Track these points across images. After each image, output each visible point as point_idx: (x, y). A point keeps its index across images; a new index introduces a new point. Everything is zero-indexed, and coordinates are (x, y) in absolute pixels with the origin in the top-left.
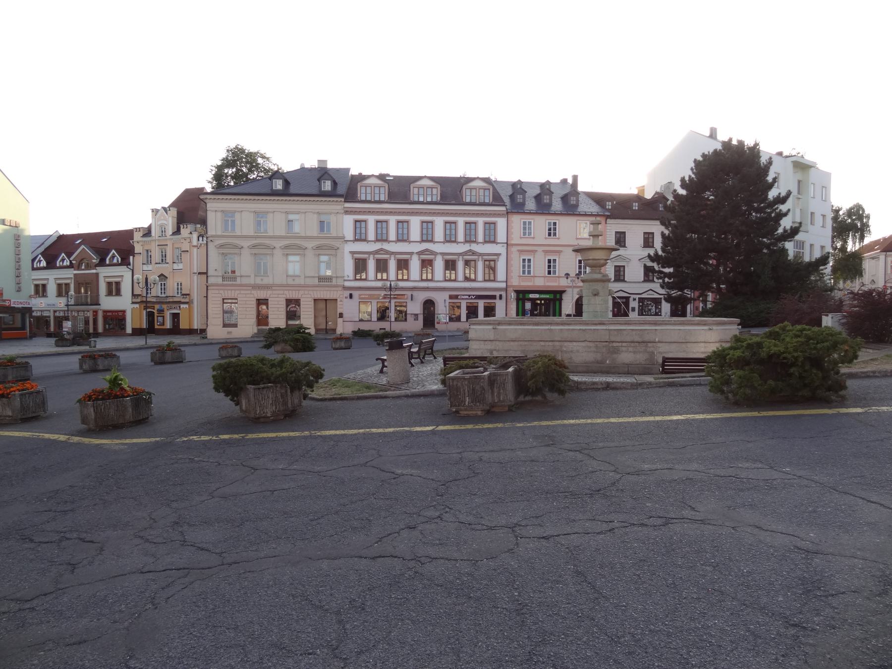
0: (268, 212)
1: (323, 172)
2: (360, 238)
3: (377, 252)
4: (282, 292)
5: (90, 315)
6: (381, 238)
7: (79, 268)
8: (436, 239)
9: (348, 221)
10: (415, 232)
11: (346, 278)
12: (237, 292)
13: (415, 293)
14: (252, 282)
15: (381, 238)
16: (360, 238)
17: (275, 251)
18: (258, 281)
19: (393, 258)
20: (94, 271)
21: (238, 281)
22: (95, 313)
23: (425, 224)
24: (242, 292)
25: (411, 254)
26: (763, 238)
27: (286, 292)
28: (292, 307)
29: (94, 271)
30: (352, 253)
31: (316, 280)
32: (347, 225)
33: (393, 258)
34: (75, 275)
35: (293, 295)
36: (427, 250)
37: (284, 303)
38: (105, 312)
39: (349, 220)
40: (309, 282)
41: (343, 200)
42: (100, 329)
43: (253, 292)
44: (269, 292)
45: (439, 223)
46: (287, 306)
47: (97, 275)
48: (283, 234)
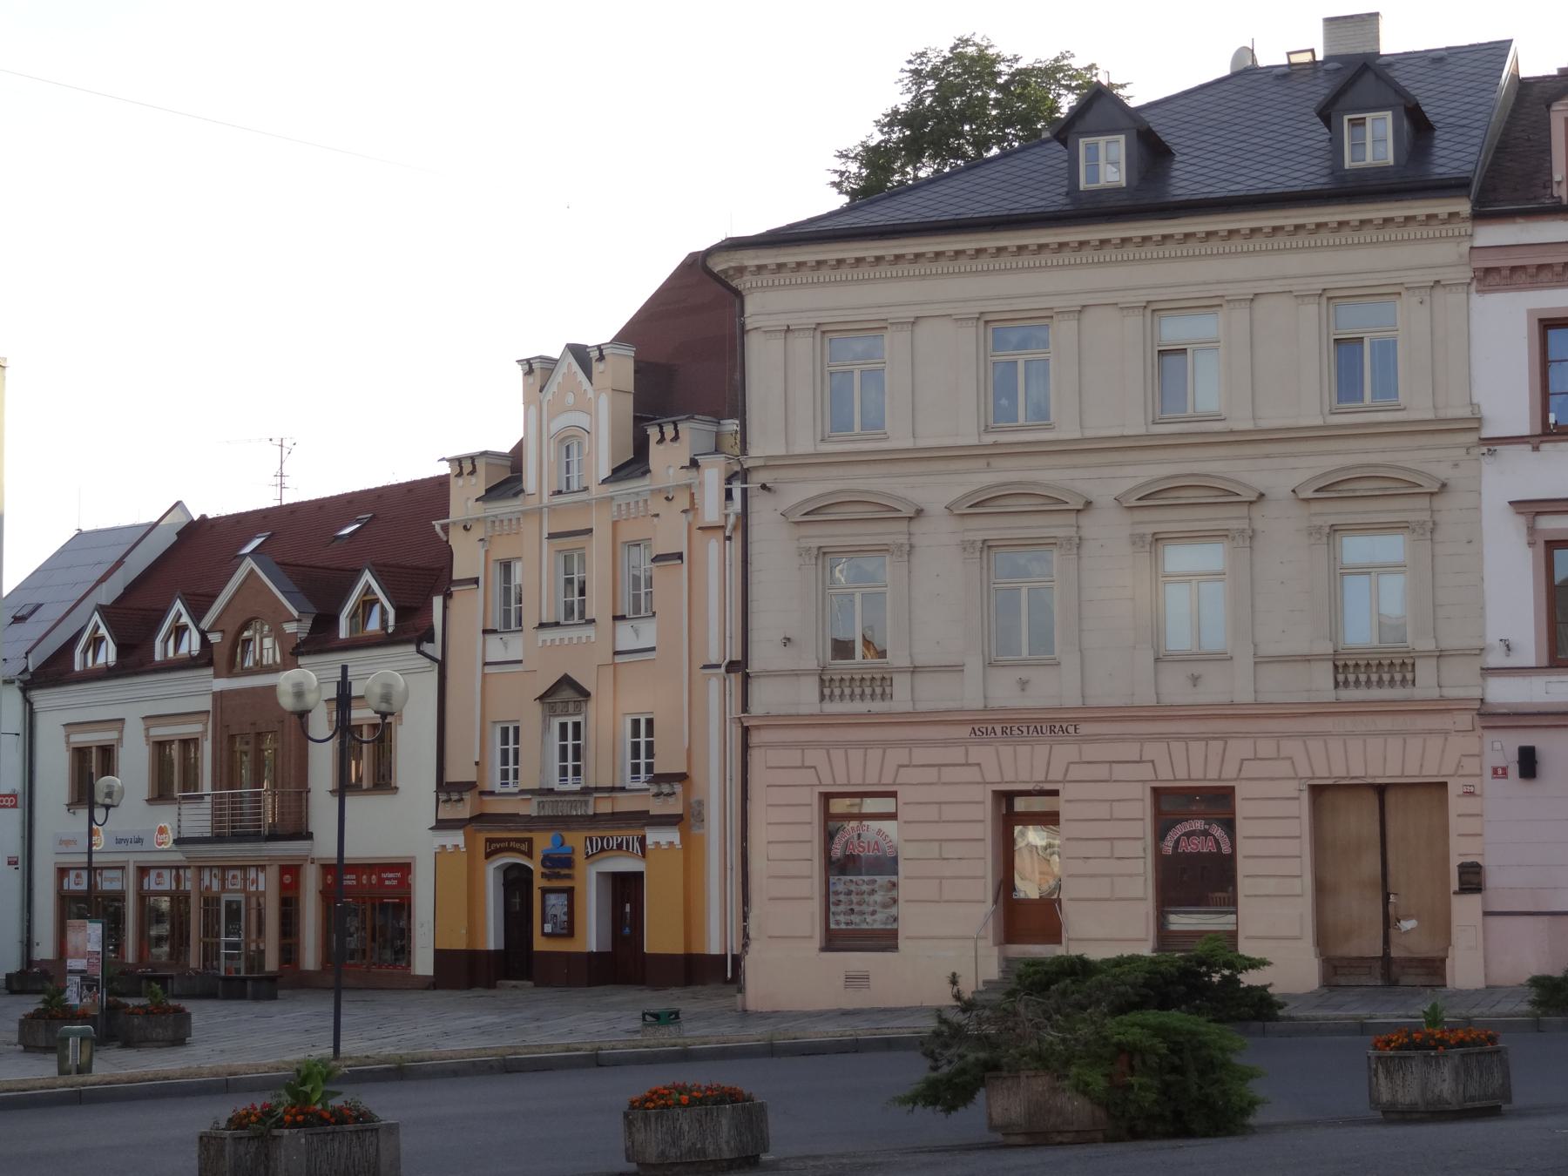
4: (1130, 751)
5: (266, 884)
11: (1496, 659)
12: (897, 756)
21: (901, 697)
22: (291, 872)
30: (1530, 509)
34: (219, 697)
35: (1193, 766)
37: (1143, 809)
40: (1281, 686)
42: (310, 958)
43: (978, 753)
44: (1065, 752)
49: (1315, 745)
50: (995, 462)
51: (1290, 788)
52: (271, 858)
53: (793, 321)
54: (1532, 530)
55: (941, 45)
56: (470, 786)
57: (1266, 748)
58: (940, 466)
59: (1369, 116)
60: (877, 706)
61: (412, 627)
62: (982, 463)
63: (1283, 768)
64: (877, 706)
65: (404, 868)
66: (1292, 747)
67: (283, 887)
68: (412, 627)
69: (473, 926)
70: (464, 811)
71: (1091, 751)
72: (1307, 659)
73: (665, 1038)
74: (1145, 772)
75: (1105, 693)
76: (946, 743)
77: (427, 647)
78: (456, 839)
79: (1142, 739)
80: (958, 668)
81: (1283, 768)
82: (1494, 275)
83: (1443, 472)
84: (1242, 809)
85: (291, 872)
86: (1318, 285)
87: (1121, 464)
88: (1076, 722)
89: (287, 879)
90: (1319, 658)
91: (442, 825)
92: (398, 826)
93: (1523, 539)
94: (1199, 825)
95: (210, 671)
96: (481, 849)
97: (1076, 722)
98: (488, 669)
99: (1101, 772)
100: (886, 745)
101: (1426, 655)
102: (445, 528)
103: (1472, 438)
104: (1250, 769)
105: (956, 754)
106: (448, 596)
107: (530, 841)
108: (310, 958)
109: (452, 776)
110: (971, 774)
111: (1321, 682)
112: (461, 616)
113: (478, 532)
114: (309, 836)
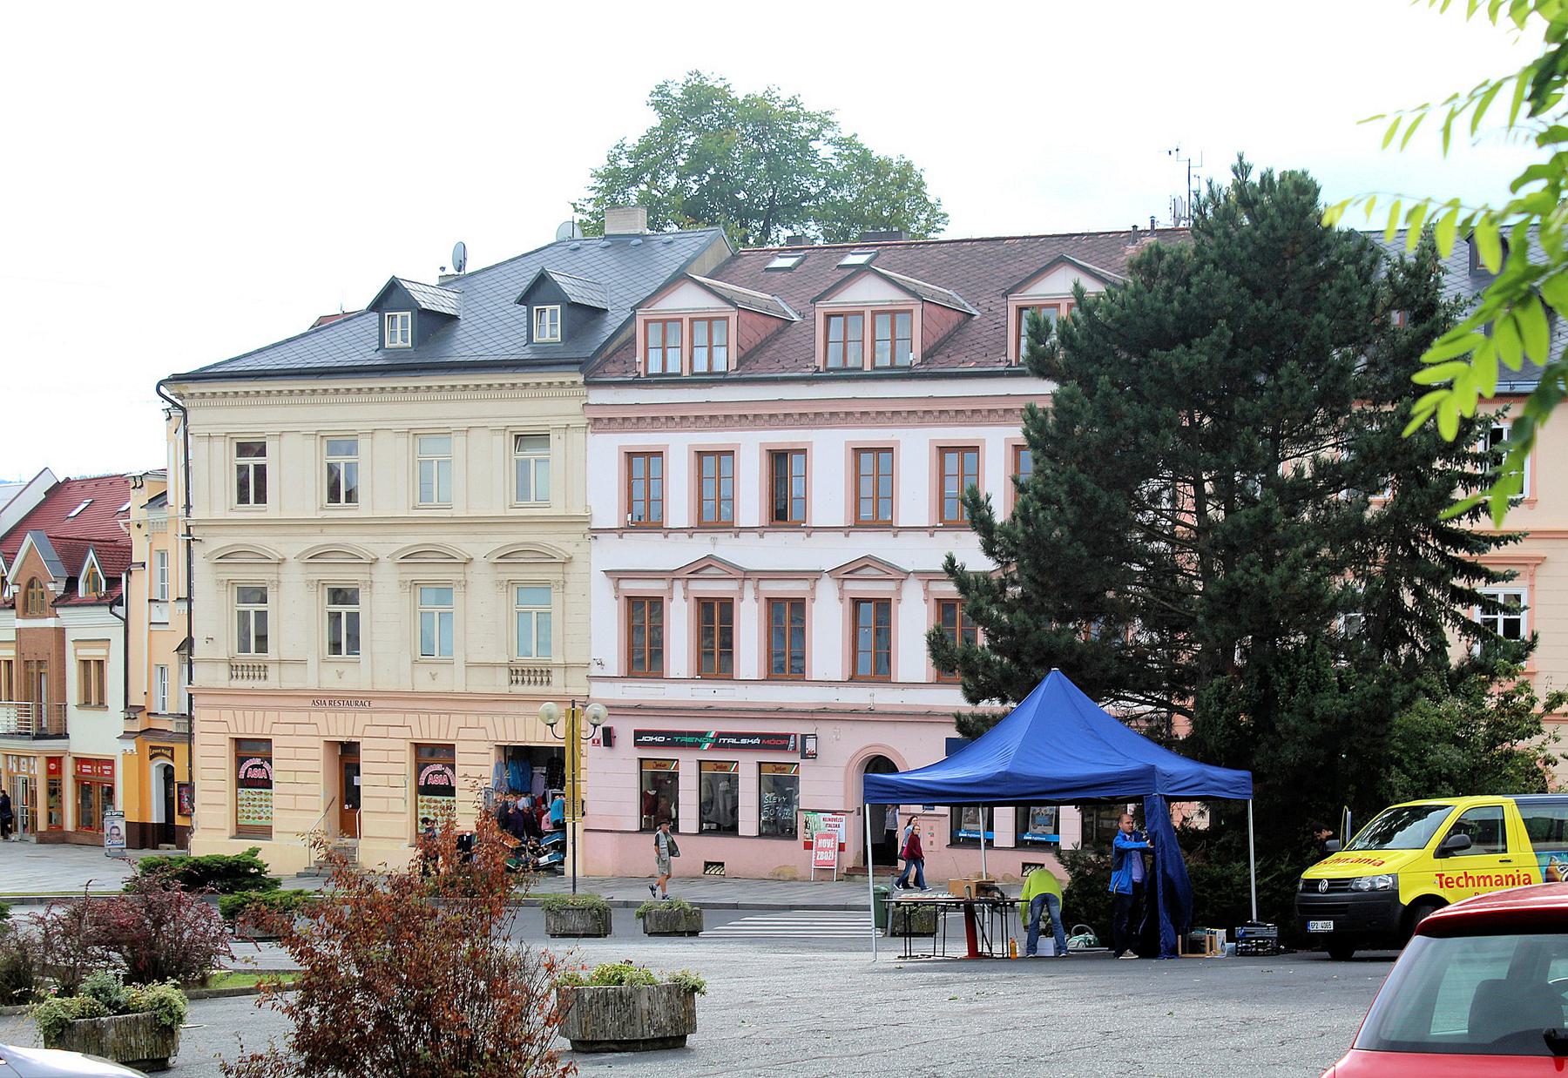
0: (447, 434)
1: (322, 320)
2: (644, 517)
3: (697, 570)
4: (397, 719)
5: (39, 770)
6: (714, 517)
7: (26, 612)
8: (816, 519)
9: (604, 456)
10: (827, 489)
11: (595, 671)
12: (272, 716)
13: (826, 731)
14: (311, 683)
15: (714, 517)
16: (644, 517)
17: (284, 569)
18: (424, 683)
19: (749, 593)
20: (51, 623)
21: (273, 681)
22: (55, 762)
23: (867, 459)
24: (287, 716)
25: (814, 576)
26: (1130, 562)
27: (411, 719)
28: (431, 774)
29: (51, 623)
30: (617, 576)
31: (503, 676)
32: (592, 471)
33: (749, 593)
34: (19, 631)
35: (433, 731)
36: (867, 562)
37: (407, 758)
38: (80, 761)
39: (606, 451)
40: (484, 683)
41: (580, 379)
42: (69, 823)
43: (318, 717)
44: (363, 718)
45: (915, 450)
46: (240, 760)
47: (60, 632)
48: (498, 511)
49: (499, 720)
50: (326, 530)
51: (484, 747)
52: (39, 752)
53: (213, 431)
54: (617, 588)
55: (677, 79)
56: (142, 708)
57: (472, 721)
58: (295, 530)
59: (548, 308)
60: (258, 684)
61: (113, 597)
62: (318, 530)
63: (480, 734)
64: (258, 684)
65: (111, 762)
66: (485, 721)
67: (50, 772)
68: (113, 597)
69: (143, 808)
70: (137, 727)
71: (379, 718)
72: (494, 665)
73: (1267, 977)
74: (406, 733)
75: (386, 683)
76: (298, 710)
77: (117, 609)
78: (131, 746)
79: (406, 712)
80: (303, 662)
81: (480, 734)
82: (601, 423)
83: (570, 549)
84: (459, 759)
85: (55, 762)
86: (502, 423)
87: (395, 534)
88: (370, 700)
89: (53, 767)
90: (501, 665)
91: (127, 735)
92: (96, 733)
93: (613, 594)
94: (439, 767)
95: (14, 613)
96: (148, 753)
97: (370, 700)
98: (153, 627)
99: (382, 731)
100: (265, 709)
101: (558, 666)
102: (127, 525)
103: (585, 528)
104: (464, 734)
105: (303, 717)
106: (129, 573)
107: (172, 749)
108: (69, 823)
109: (131, 703)
110: (312, 730)
111: (500, 683)
112: (138, 587)
113: (145, 530)
114: (66, 736)
